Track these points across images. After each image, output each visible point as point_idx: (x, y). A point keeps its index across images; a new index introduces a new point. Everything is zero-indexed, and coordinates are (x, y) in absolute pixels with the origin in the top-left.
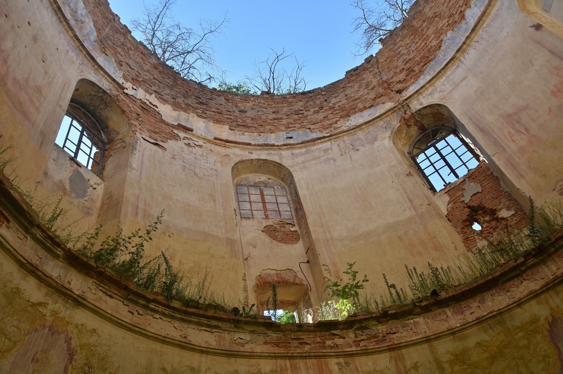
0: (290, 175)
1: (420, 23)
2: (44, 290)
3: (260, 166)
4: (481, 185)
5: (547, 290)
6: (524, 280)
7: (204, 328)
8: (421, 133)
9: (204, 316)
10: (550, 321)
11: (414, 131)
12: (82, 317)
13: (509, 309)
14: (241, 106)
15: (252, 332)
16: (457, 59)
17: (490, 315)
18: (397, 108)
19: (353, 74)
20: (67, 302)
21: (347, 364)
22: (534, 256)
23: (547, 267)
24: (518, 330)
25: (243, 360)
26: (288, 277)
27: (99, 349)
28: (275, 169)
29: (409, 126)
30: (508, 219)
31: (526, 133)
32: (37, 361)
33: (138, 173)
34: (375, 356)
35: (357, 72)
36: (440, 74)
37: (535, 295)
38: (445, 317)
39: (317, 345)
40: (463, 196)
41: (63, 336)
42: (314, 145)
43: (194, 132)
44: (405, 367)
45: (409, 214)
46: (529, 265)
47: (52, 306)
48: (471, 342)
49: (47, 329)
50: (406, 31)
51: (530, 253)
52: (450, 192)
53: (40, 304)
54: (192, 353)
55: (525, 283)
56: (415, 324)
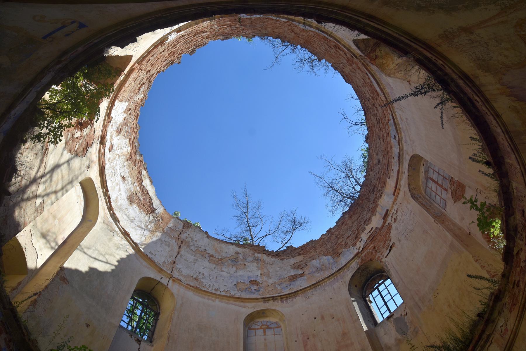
1: (301, 39)
3: (414, 169)
7: (487, 346)
9: (478, 341)
14: (376, 162)
15: (500, 314)
19: (347, 79)
29: (377, 57)
42: (399, 124)
43: (389, 209)
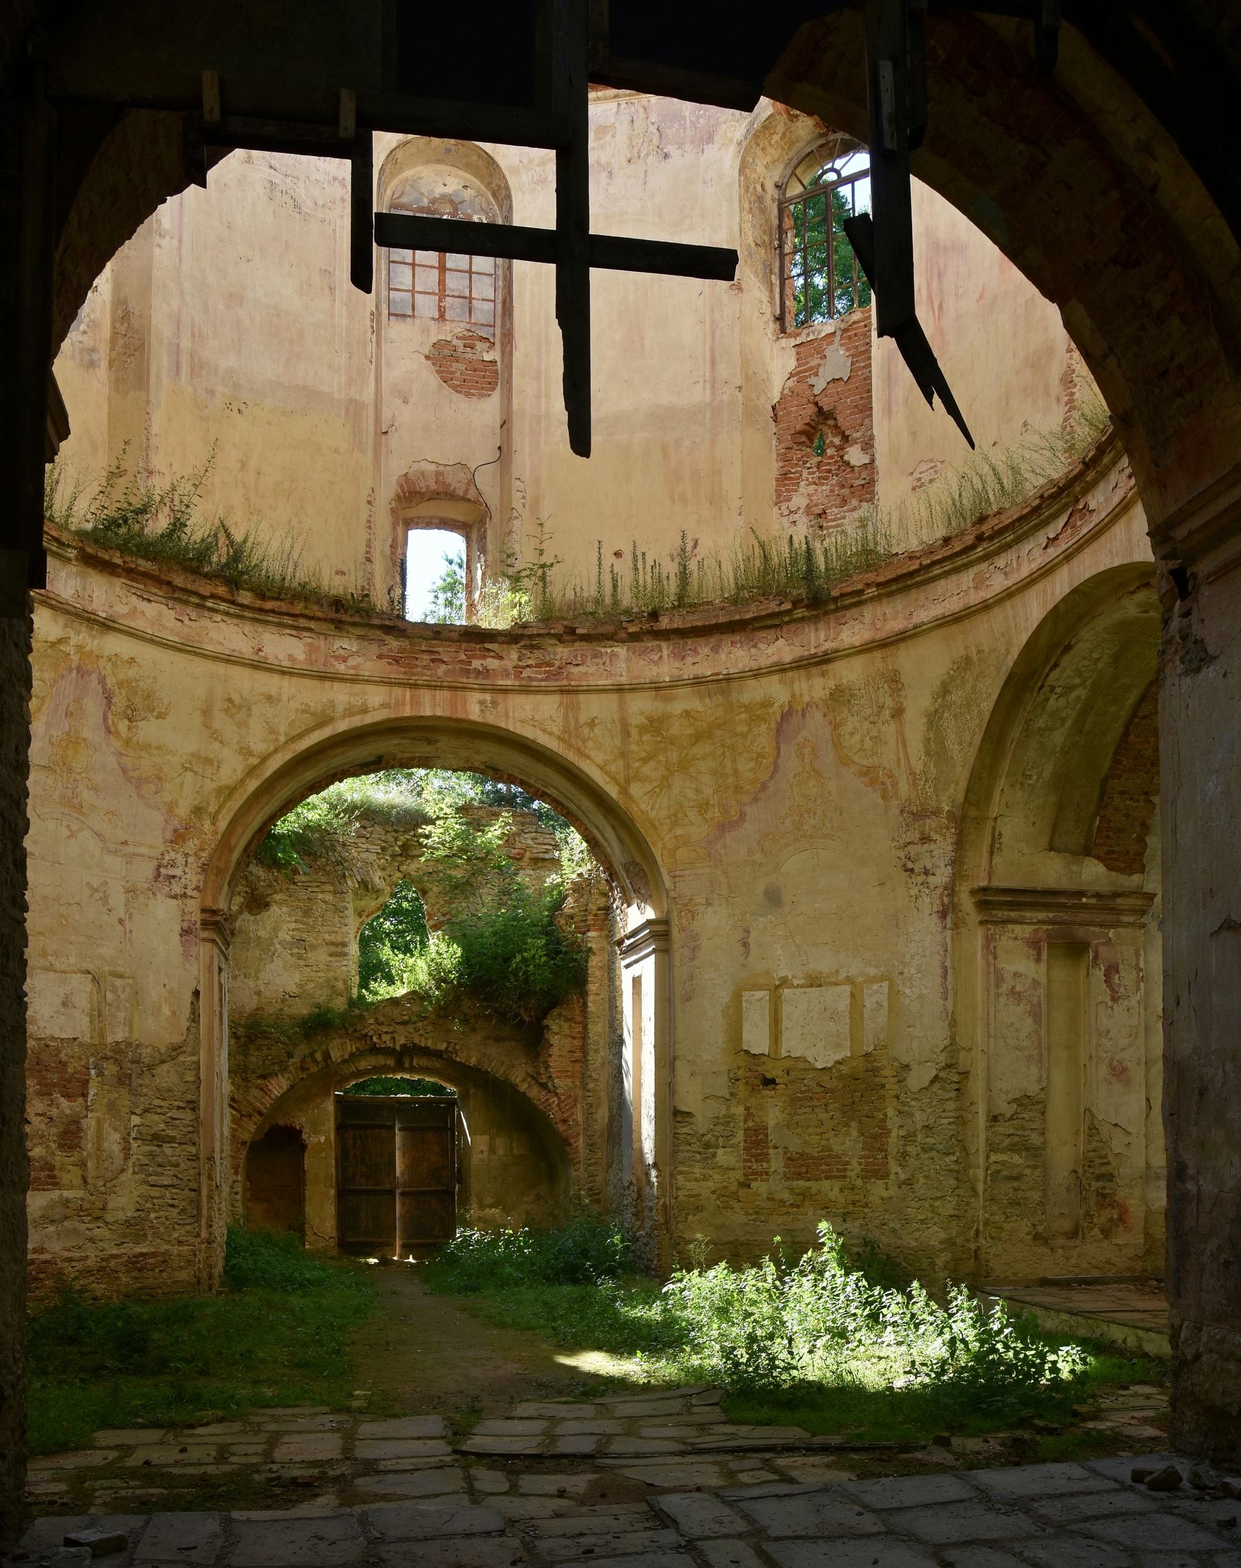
0: (509, 197)
2: (62, 620)
4: (853, 363)
5: (798, 667)
8: (822, 135)
12: (114, 644)
13: (741, 677)
20: (92, 629)
21: (494, 703)
22: (806, 606)
25: (343, 685)
26: (457, 482)
27: (141, 683)
28: (480, 163)
32: (72, 714)
33: (175, 243)
34: (540, 697)
37: (781, 669)
38: (656, 658)
39: (457, 667)
40: (816, 375)
41: (94, 676)
44: (577, 721)
45: (700, 395)
47: (75, 639)
48: (677, 708)
49: (75, 672)
52: (802, 349)
53: (60, 641)
54: (268, 674)
56: (614, 656)
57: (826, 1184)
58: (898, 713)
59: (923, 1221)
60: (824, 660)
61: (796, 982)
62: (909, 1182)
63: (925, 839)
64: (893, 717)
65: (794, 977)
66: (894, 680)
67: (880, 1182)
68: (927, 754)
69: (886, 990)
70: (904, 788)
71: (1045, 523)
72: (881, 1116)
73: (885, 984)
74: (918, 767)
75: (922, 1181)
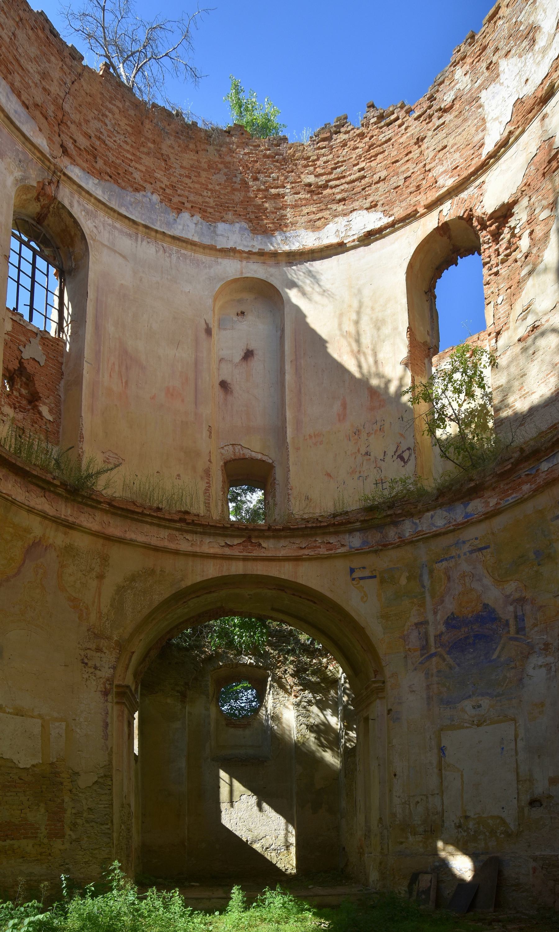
5: (54, 521)
6: (45, 496)
10: (36, 541)
11: (34, 208)
13: (20, 506)
16: (137, 229)
17: (6, 496)
18: (48, 164)
23: (66, 506)
24: (12, 526)
29: (37, 199)
30: (45, 420)
31: (124, 384)
35: (51, 37)
36: (112, 213)
37: (44, 516)
46: (57, 491)
50: (132, 112)
51: (66, 485)
55: (43, 499)
57: (24, 842)
58: (101, 577)
59: (86, 863)
60: (70, 526)
61: (8, 710)
62: (78, 840)
63: (99, 650)
64: (97, 577)
65: (6, 706)
66: (105, 559)
67: (59, 841)
68: (111, 605)
69: (64, 727)
70: (93, 617)
71: (232, 536)
72: (59, 801)
73: (64, 724)
74: (105, 610)
75: (86, 839)
